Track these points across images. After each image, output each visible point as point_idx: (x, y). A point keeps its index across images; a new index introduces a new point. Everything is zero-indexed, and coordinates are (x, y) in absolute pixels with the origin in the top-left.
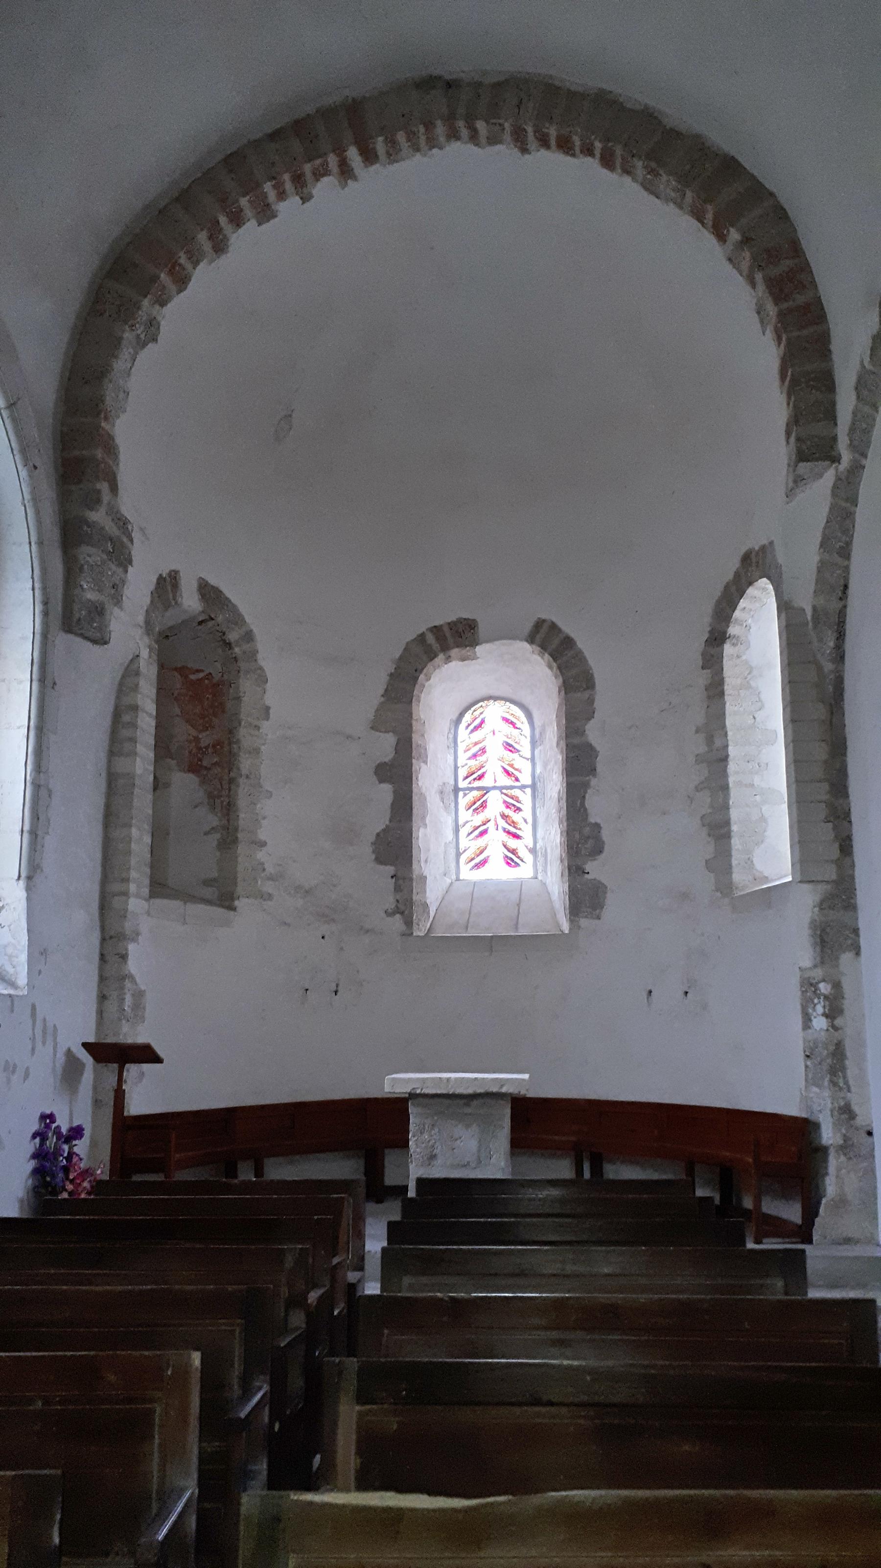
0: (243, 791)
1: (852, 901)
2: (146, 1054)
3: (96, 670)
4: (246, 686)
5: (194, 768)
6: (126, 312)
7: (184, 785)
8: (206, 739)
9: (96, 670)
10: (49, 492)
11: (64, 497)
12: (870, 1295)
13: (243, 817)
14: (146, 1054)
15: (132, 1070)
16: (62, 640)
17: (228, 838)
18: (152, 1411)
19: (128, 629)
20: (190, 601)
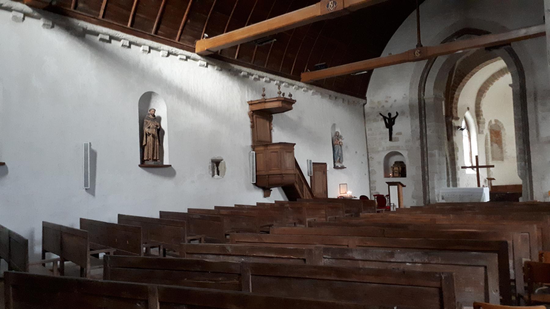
0: (503, 145)
1: (526, 285)
2: (494, 179)
3: (483, 137)
4: (502, 131)
5: (496, 143)
6: (482, 96)
7: (495, 145)
8: (497, 139)
9: (483, 137)
10: (475, 119)
11: (477, 118)
12: (502, 306)
13: (504, 149)
14: (494, 179)
15: (492, 181)
16: (479, 135)
17: (502, 152)
18: (250, 61)
19: (486, 131)
20: (493, 122)
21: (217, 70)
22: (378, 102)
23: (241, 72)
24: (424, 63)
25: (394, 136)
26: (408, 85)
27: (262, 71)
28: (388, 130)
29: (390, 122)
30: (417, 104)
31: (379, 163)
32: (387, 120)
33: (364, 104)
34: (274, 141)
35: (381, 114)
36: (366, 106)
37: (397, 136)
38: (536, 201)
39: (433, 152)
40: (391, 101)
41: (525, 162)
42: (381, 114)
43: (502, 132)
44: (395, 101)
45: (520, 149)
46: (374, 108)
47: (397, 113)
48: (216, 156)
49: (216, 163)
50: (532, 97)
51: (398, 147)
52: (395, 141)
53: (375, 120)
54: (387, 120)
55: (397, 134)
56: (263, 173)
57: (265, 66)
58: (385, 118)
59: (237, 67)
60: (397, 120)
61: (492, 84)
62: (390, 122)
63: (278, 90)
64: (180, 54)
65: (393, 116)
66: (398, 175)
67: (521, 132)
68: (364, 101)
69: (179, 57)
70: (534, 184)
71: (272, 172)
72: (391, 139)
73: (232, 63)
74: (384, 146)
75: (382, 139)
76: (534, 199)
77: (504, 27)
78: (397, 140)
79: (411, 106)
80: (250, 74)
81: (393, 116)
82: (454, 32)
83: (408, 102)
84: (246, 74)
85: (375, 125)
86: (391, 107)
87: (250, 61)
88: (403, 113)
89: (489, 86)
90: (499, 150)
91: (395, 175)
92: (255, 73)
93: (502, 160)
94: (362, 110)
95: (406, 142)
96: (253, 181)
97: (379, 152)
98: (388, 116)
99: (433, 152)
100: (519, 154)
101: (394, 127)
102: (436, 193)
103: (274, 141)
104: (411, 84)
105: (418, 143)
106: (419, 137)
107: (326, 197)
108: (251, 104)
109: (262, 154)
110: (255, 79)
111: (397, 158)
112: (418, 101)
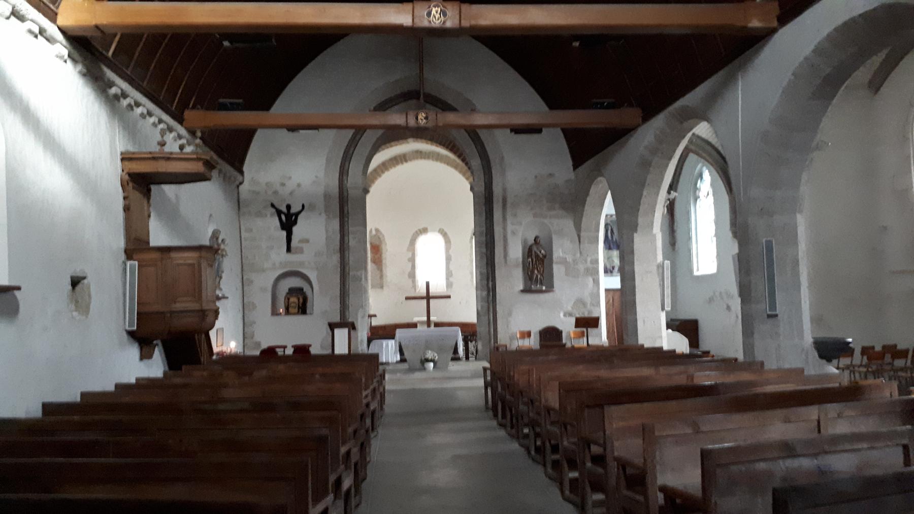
2: (375, 316)
14: (375, 316)
15: (373, 319)
17: (381, 277)
21: (80, 72)
22: (267, 184)
23: (111, 87)
24: (350, 133)
25: (294, 243)
26: (323, 161)
27: (141, 92)
28: (284, 233)
29: (288, 221)
30: (338, 195)
31: (263, 290)
32: (283, 217)
33: (241, 183)
34: (153, 243)
35: (273, 206)
36: (241, 187)
37: (300, 245)
38: (643, 346)
39: (359, 273)
40: (291, 185)
41: (489, 292)
42: (273, 206)
43: (383, 246)
44: (299, 185)
45: (481, 274)
46: (258, 193)
47: (303, 206)
48: (77, 269)
49: (75, 282)
50: (501, 204)
51: (302, 264)
52: (296, 253)
53: (259, 214)
54: (283, 217)
55: (301, 241)
56: (156, 308)
57: (145, 83)
58: (279, 213)
59: (110, 74)
60: (301, 219)
61: (380, 176)
62: (288, 221)
63: (159, 138)
64: (32, 21)
65: (293, 210)
66: (296, 310)
67: (484, 250)
68: (240, 178)
69: (28, 25)
70: (499, 322)
71: (179, 306)
72: (289, 249)
73: (109, 67)
74: (278, 258)
75: (272, 248)
76: (625, 343)
77: (468, 100)
78: (301, 251)
79: (327, 196)
80: (124, 95)
81: (293, 210)
82: (399, 92)
83: (321, 190)
84: (119, 92)
85: (259, 223)
86: (291, 193)
87: (127, 67)
88: (313, 207)
89: (376, 179)
90: (378, 272)
91: (291, 310)
92: (132, 95)
93: (382, 287)
94: (236, 195)
95: (315, 255)
96: (131, 325)
97: (263, 271)
98: (284, 209)
99: (359, 273)
100: (481, 280)
101: (295, 229)
102: (359, 339)
103: (153, 243)
104: (328, 161)
105: (336, 258)
106: (338, 247)
107: (329, 351)
108: (126, 158)
109: (152, 269)
110: (130, 106)
111: (295, 282)
112: (337, 190)
